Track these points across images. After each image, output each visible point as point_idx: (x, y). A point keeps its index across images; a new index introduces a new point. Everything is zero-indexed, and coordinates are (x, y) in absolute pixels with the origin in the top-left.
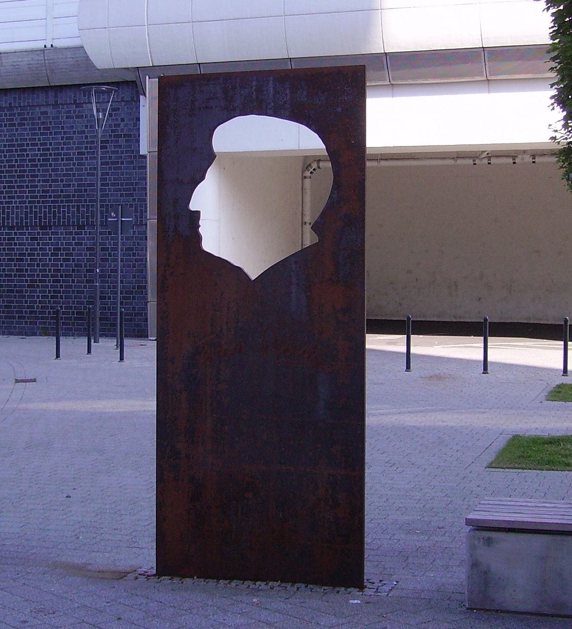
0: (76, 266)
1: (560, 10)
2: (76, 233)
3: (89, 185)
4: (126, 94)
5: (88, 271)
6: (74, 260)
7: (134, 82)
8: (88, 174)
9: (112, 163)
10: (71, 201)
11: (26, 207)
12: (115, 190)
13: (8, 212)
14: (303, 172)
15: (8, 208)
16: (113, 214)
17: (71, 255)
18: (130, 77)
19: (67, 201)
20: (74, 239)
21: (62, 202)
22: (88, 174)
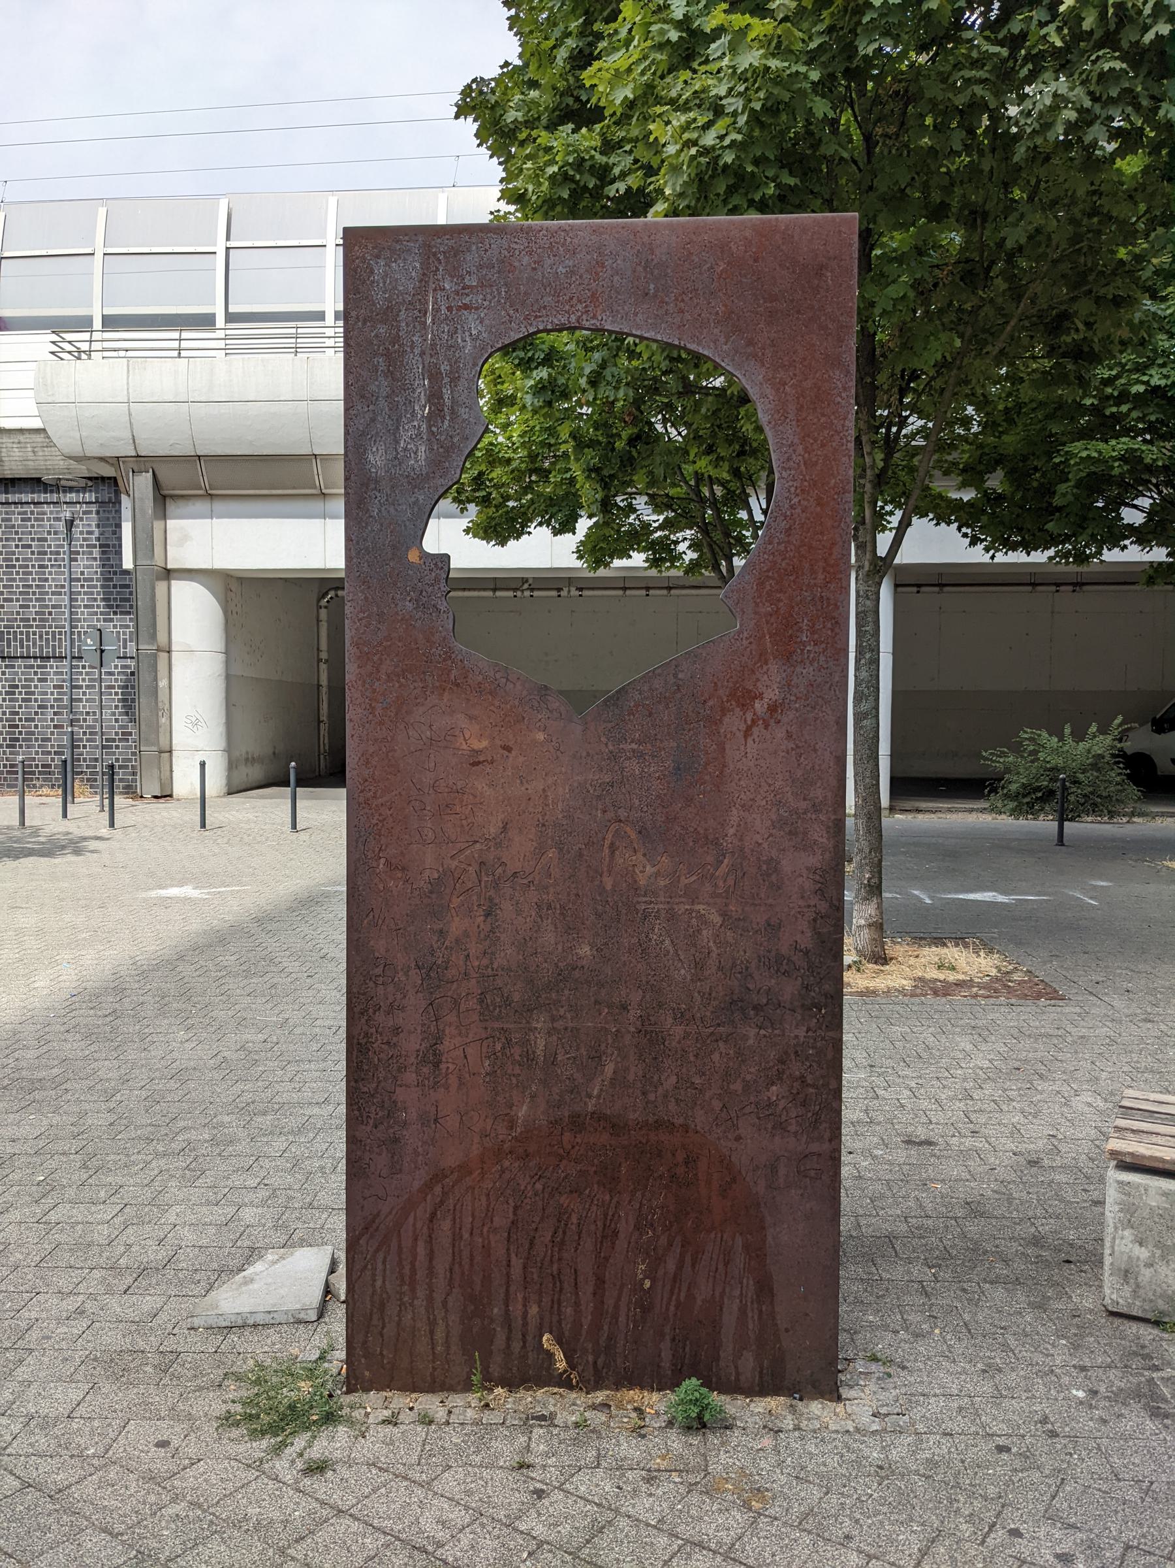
0: (40, 707)
1: (987, 127)
2: (39, 667)
3: (54, 607)
4: (106, 494)
5: (55, 714)
6: (36, 700)
7: (44, 430)
8: (53, 593)
9: (85, 580)
10: (31, 627)
11: (22, 634)
12: (90, 614)
13: (60, 639)
14: (319, 600)
15: (60, 633)
16: (89, 641)
17: (33, 693)
18: (107, 471)
19: (25, 627)
20: (36, 673)
21: (19, 627)
22: (53, 593)
